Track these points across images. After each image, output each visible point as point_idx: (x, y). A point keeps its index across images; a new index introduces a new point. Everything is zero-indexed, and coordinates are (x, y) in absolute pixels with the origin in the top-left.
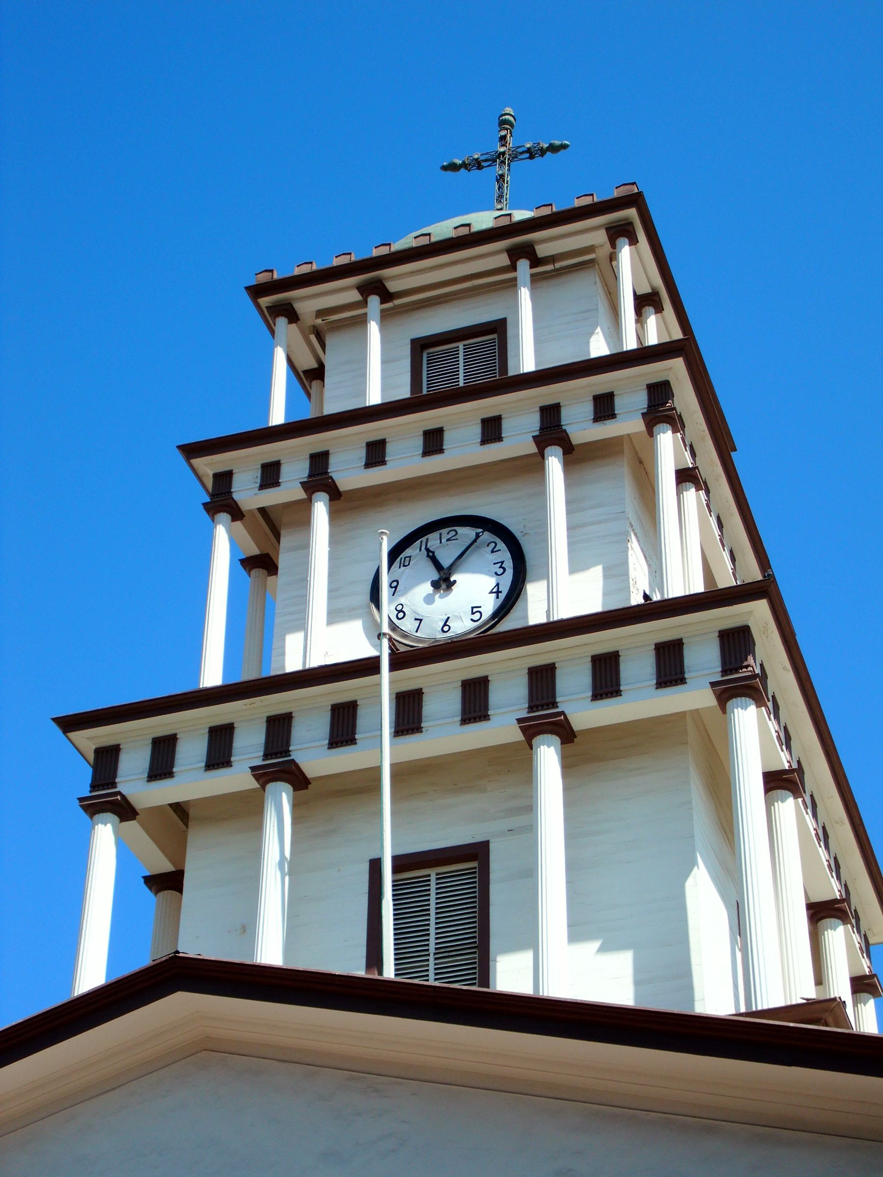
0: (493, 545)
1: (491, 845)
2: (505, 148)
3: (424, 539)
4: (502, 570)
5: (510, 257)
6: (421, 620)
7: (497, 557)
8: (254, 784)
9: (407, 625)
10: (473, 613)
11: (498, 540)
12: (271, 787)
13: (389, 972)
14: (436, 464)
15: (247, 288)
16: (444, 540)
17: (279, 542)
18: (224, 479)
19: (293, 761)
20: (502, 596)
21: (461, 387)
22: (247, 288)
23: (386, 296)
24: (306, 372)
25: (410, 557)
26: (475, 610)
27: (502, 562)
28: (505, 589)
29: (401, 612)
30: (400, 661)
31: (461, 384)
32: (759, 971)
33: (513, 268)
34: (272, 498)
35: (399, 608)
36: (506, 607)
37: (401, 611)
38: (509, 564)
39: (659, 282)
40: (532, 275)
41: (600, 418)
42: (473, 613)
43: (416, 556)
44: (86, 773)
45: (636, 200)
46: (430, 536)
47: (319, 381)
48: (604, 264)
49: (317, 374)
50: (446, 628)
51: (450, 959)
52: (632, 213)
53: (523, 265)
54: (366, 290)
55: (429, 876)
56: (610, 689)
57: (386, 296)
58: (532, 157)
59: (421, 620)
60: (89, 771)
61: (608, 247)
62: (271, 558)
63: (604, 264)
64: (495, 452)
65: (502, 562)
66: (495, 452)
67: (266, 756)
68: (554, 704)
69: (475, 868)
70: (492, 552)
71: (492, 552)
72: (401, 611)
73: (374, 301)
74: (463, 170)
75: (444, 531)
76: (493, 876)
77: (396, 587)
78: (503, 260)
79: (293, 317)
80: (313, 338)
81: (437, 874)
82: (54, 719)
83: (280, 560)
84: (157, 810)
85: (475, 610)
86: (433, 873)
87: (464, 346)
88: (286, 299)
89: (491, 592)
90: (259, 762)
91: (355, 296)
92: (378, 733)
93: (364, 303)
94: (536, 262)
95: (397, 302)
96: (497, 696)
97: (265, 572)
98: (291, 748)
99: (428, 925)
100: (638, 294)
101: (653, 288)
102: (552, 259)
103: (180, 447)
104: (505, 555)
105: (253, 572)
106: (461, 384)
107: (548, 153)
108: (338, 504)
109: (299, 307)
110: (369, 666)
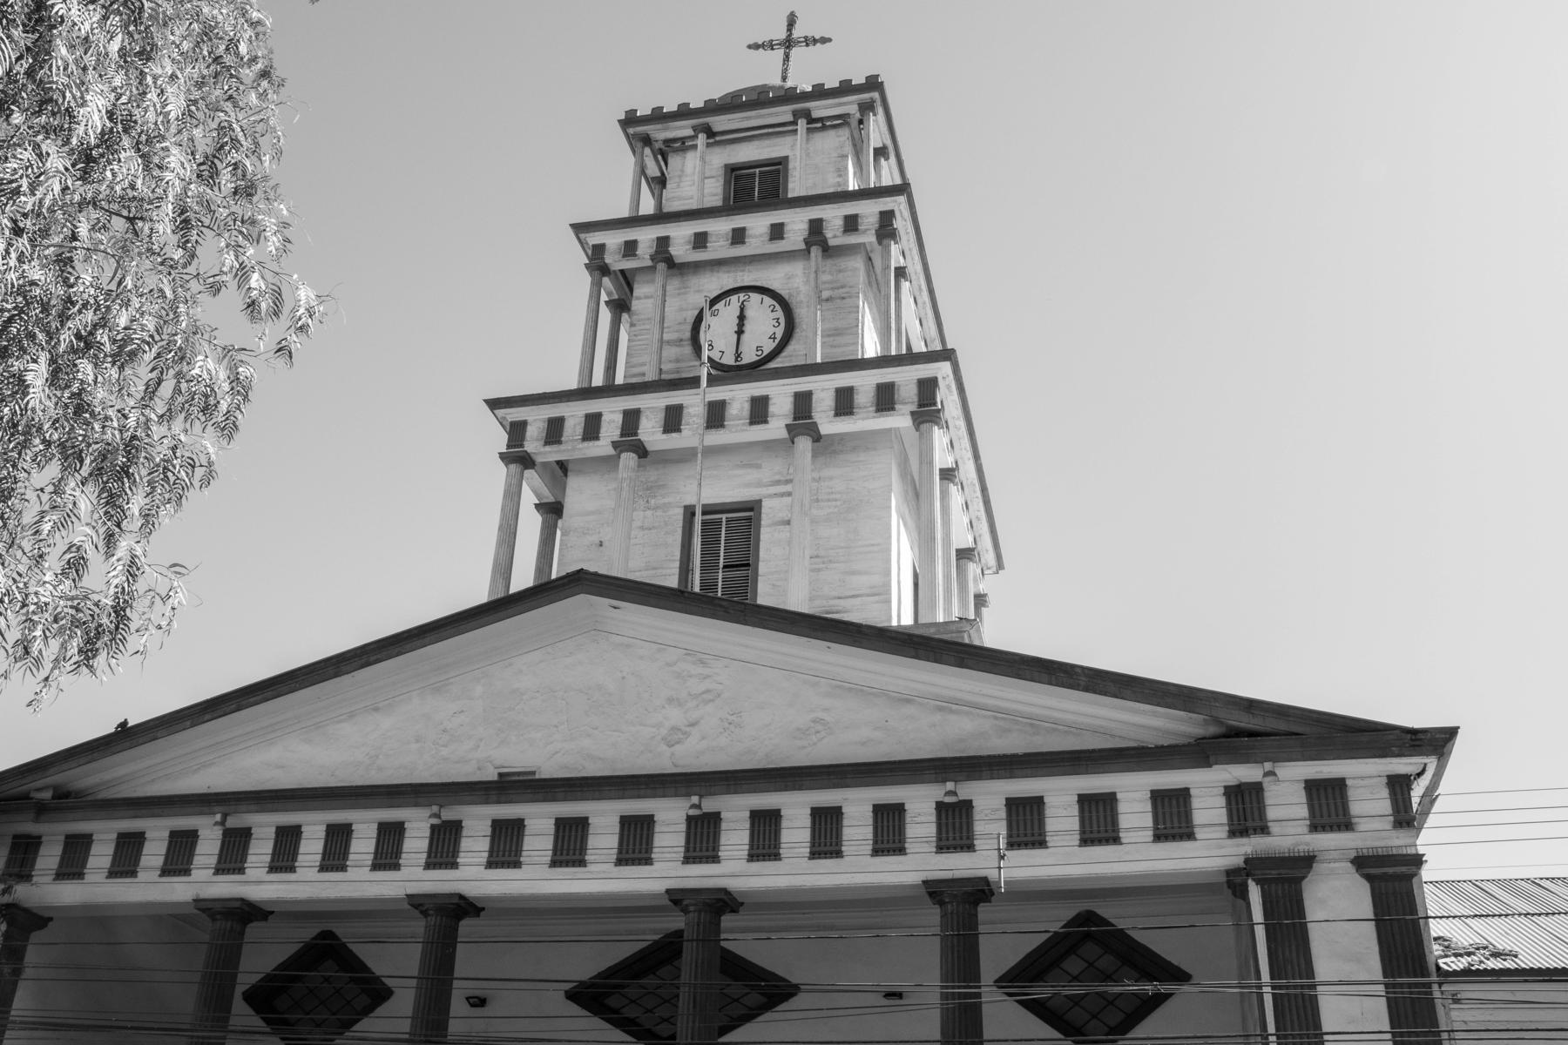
3: (728, 299)
5: (794, 116)
6: (723, 352)
7: (775, 315)
11: (777, 305)
12: (624, 456)
20: (777, 341)
23: (710, 133)
24: (653, 178)
27: (778, 319)
28: (779, 336)
32: (1537, 1030)
33: (795, 123)
34: (628, 264)
38: (782, 321)
39: (889, 143)
40: (808, 129)
44: (504, 437)
45: (873, 84)
48: (854, 123)
49: (661, 182)
50: (739, 359)
51: (1529, 946)
52: (876, 95)
58: (807, 45)
59: (723, 352)
61: (858, 115)
62: (625, 302)
65: (778, 319)
67: (622, 435)
70: (772, 311)
71: (772, 311)
74: (817, 37)
75: (741, 295)
78: (790, 118)
79: (647, 140)
80: (660, 157)
84: (545, 464)
89: (770, 338)
92: (1054, 683)
94: (811, 120)
95: (718, 138)
101: (884, 145)
107: (818, 44)
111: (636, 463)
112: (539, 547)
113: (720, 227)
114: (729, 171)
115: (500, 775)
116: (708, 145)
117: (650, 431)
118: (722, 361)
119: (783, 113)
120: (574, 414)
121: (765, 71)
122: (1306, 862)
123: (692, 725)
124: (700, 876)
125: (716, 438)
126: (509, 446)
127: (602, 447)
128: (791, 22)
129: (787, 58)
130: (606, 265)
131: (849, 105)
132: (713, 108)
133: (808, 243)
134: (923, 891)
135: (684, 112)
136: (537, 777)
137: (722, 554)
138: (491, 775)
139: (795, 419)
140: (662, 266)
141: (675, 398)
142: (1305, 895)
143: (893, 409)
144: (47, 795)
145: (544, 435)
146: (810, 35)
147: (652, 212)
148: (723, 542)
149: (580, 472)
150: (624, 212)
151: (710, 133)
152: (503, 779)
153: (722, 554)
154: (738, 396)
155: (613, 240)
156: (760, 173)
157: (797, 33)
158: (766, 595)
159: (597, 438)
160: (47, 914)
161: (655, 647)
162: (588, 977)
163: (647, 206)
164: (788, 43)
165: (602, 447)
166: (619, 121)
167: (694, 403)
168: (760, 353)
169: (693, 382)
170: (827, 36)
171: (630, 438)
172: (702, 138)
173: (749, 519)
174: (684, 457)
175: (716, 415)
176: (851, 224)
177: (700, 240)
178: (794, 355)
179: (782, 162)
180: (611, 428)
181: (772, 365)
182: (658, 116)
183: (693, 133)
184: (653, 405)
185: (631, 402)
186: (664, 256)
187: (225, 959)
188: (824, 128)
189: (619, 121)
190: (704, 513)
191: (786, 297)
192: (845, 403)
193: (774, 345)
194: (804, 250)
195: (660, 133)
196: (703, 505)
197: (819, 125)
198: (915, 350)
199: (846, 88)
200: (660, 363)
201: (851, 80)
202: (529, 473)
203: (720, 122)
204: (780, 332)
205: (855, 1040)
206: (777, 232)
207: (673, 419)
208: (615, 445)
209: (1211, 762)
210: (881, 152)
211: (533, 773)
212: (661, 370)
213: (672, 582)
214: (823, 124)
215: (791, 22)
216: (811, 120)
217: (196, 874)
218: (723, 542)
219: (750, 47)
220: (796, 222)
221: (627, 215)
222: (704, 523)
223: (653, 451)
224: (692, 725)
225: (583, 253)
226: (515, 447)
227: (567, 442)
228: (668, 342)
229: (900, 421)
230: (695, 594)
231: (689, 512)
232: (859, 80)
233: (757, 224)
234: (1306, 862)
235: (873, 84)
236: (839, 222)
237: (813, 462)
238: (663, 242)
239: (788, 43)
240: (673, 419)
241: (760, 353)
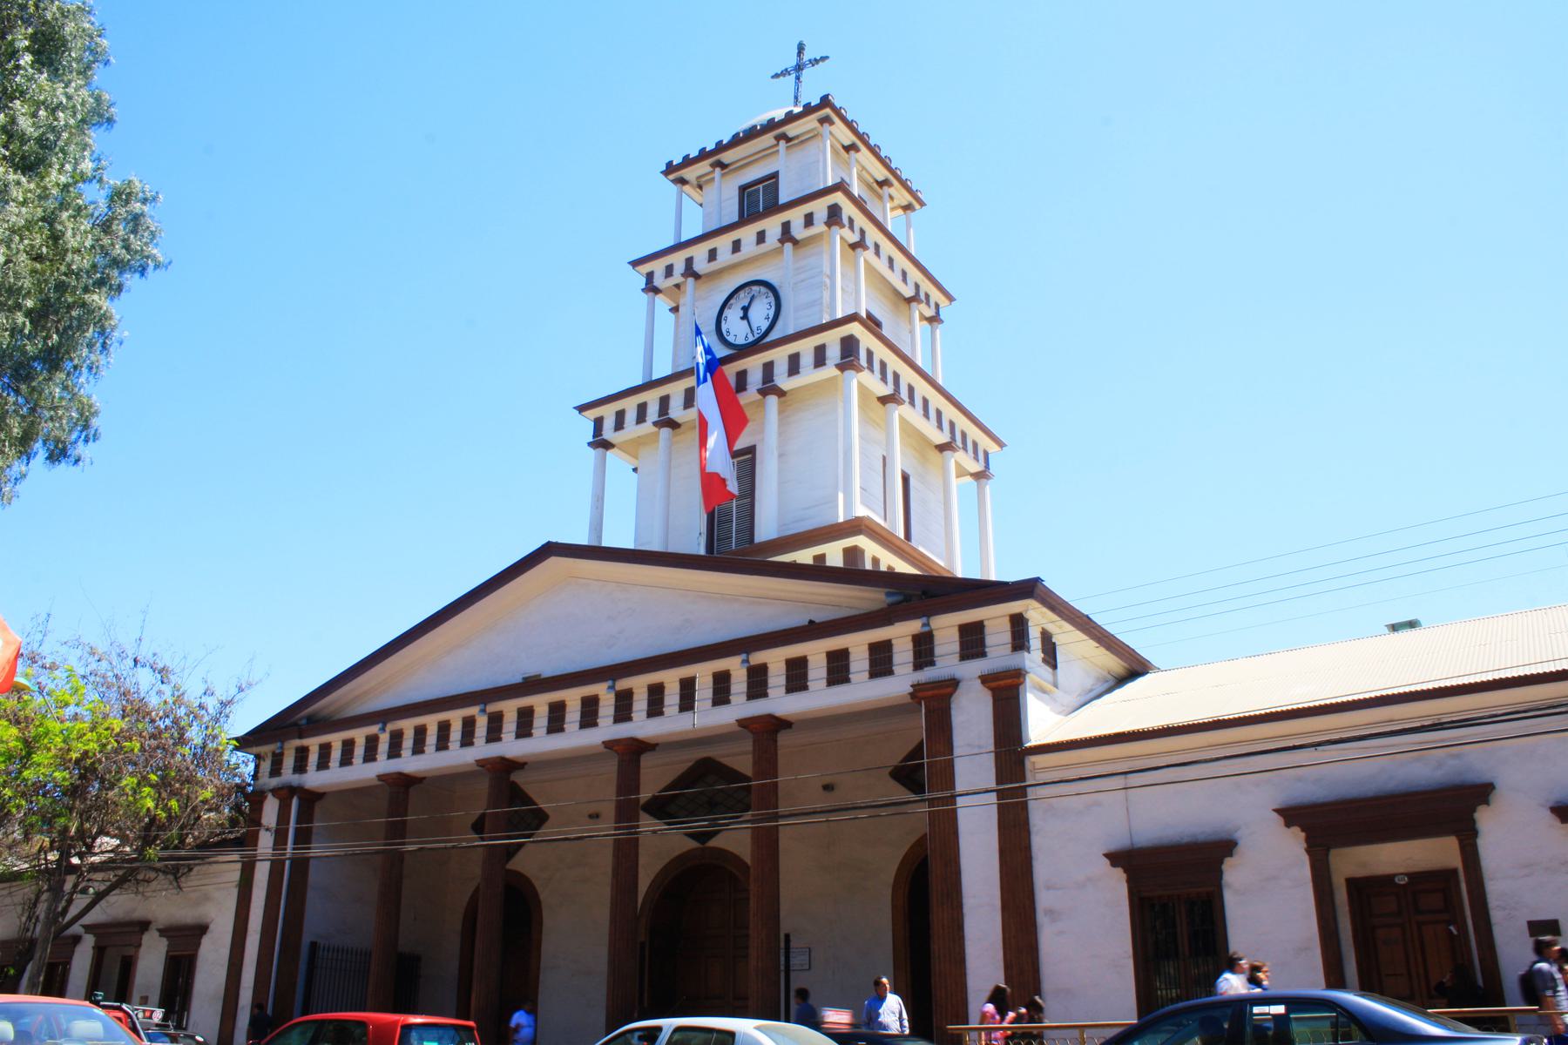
2: (62, 432)
15: (662, 172)
18: (650, 276)
19: (775, 385)
20: (770, 320)
22: (662, 172)
23: (723, 166)
28: (771, 316)
38: (773, 304)
52: (827, 111)
54: (778, 138)
57: (788, 140)
66: (763, 248)
73: (782, 143)
74: (818, 58)
78: (773, 142)
88: (679, 176)
90: (592, 440)
91: (709, 169)
93: (778, 144)
95: (731, 167)
102: (797, 137)
103: (629, 263)
104: (772, 299)
113: (747, 234)
115: (524, 678)
116: (723, 175)
119: (768, 139)
122: (953, 684)
124: (759, 708)
126: (594, 437)
128: (801, 49)
129: (798, 78)
132: (721, 148)
133: (782, 241)
134: (603, 746)
135: (704, 155)
138: (518, 679)
142: (953, 706)
143: (825, 364)
144: (304, 722)
146: (812, 58)
151: (723, 166)
156: (764, 187)
157: (807, 56)
160: (521, 761)
162: (900, 758)
164: (799, 68)
170: (824, 55)
176: (809, 220)
177: (713, 255)
178: (786, 327)
180: (653, 413)
181: (768, 339)
182: (688, 162)
187: (628, 779)
191: (777, 288)
192: (794, 366)
195: (690, 173)
198: (719, 355)
201: (810, 103)
202: (610, 454)
203: (727, 157)
204: (772, 313)
205: (1297, 769)
208: (655, 424)
215: (801, 49)
217: (940, 662)
229: (829, 371)
234: (953, 684)
236: (802, 221)
238: (689, 262)
239: (799, 68)
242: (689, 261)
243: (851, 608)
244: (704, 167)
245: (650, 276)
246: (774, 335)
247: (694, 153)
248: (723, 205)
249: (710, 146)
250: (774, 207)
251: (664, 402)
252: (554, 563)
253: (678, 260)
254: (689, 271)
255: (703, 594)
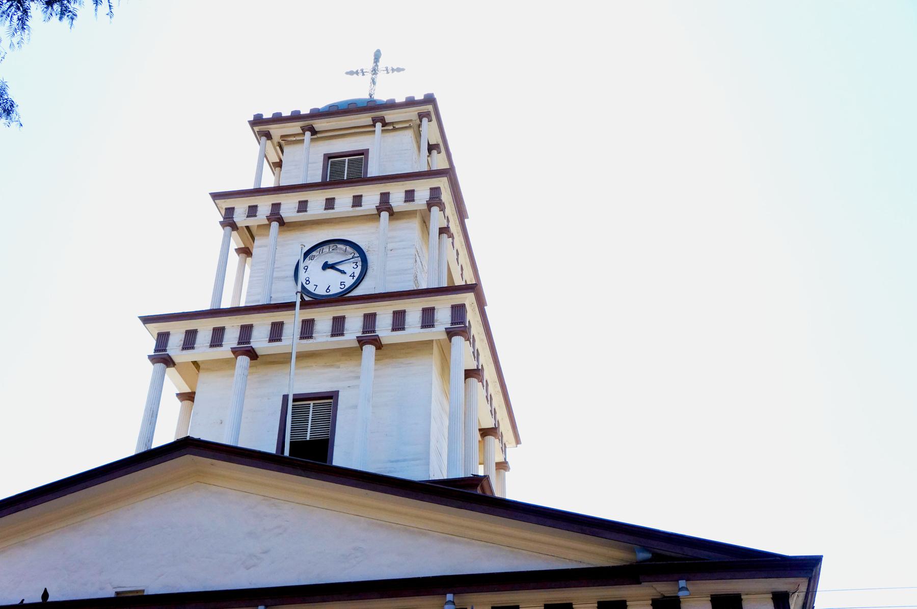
0: (353, 254)
1: (340, 393)
4: (356, 266)
5: (373, 120)
6: (317, 286)
8: (232, 356)
9: (310, 288)
10: (341, 285)
11: (355, 252)
12: (240, 358)
13: (287, 453)
14: (330, 214)
16: (331, 250)
17: (254, 242)
20: (355, 278)
21: (307, 441)
23: (314, 132)
24: (273, 163)
25: (314, 256)
26: (342, 283)
28: (357, 275)
29: (308, 281)
30: (304, 305)
31: (308, 439)
33: (374, 126)
34: (252, 222)
35: (307, 279)
36: (397, 335)
37: (308, 281)
38: (360, 264)
41: (214, 345)
42: (341, 285)
43: (317, 256)
45: (430, 100)
46: (324, 247)
47: (279, 168)
49: (279, 165)
50: (328, 291)
52: (430, 108)
53: (379, 125)
55: (310, 404)
56: (400, 327)
59: (317, 286)
60: (154, 342)
61: (418, 121)
62: (249, 250)
63: (416, 128)
64: (358, 211)
65: (357, 263)
66: (358, 211)
67: (239, 343)
68: (374, 331)
69: (331, 402)
72: (308, 281)
74: (355, 75)
75: (331, 245)
76: (339, 407)
77: (307, 269)
79: (268, 136)
80: (278, 148)
81: (314, 404)
82: (139, 317)
83: (254, 251)
85: (342, 283)
86: (312, 403)
87: (314, 404)
89: (350, 276)
90: (235, 346)
93: (304, 134)
94: (385, 124)
95: (319, 135)
96: (348, 324)
97: (246, 255)
98: (251, 341)
99: (307, 427)
100: (430, 144)
102: (392, 123)
103: (210, 194)
105: (240, 255)
106: (345, 178)
108: (283, 228)
109: (272, 132)
110: (290, 306)
111: (249, 364)
112: (178, 424)
113: (316, 201)
114: (327, 158)
115: (117, 593)
117: (260, 341)
118: (315, 292)
119: (365, 119)
120: (205, 329)
121: (358, 91)
123: (265, 552)
125: (308, 345)
126: (156, 351)
127: (224, 352)
128: (377, 56)
130: (235, 222)
131: (411, 113)
132: (316, 114)
135: (296, 117)
136: (145, 593)
137: (309, 430)
139: (363, 333)
140: (275, 225)
141: (278, 317)
145: (182, 342)
147: (320, 181)
148: (310, 421)
149: (208, 370)
150: (251, 186)
151: (314, 132)
152: (119, 596)
153: (309, 430)
154: (323, 318)
155: (241, 206)
157: (382, 64)
158: (339, 459)
159: (221, 345)
161: (263, 498)
163: (269, 181)
165: (224, 352)
166: (249, 122)
167: (292, 321)
168: (343, 286)
169: (290, 306)
170: (401, 67)
171: (369, 338)
172: (308, 134)
173: (329, 404)
174: (283, 360)
175: (307, 329)
179: (364, 153)
180: (231, 338)
182: (278, 119)
183: (301, 132)
184: (262, 325)
185: (246, 320)
186: (276, 217)
188: (395, 129)
189: (249, 122)
190: (294, 400)
191: (365, 251)
193: (353, 281)
194: (376, 214)
195: (277, 131)
196: (294, 395)
197: (391, 127)
199: (410, 103)
200: (271, 293)
202: (171, 371)
203: (319, 124)
206: (357, 201)
207: (276, 332)
209: (641, 581)
210: (431, 148)
211: (143, 591)
212: (271, 297)
213: (272, 449)
214: (394, 127)
215: (377, 56)
216: (385, 124)
218: (310, 421)
219: (347, 73)
220: (371, 196)
221: (252, 188)
222: (294, 407)
223: (386, 345)
224: (265, 552)
225: (220, 215)
226: (243, 343)
227: (199, 347)
228: (278, 278)
230: (286, 458)
231: (285, 398)
232: (419, 97)
233: (343, 197)
235: (430, 100)
237: (376, 364)
238: (276, 207)
240: (276, 332)
241: (343, 286)
242: (276, 207)
243: (589, 564)
244: (294, 128)
245: (230, 212)
246: (357, 292)
247: (286, 113)
248: (309, 165)
249: (267, 115)
250: (359, 178)
251: (246, 331)
252: (187, 460)
253: (264, 205)
254: (275, 215)
255: (383, 523)
